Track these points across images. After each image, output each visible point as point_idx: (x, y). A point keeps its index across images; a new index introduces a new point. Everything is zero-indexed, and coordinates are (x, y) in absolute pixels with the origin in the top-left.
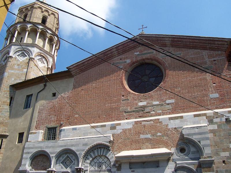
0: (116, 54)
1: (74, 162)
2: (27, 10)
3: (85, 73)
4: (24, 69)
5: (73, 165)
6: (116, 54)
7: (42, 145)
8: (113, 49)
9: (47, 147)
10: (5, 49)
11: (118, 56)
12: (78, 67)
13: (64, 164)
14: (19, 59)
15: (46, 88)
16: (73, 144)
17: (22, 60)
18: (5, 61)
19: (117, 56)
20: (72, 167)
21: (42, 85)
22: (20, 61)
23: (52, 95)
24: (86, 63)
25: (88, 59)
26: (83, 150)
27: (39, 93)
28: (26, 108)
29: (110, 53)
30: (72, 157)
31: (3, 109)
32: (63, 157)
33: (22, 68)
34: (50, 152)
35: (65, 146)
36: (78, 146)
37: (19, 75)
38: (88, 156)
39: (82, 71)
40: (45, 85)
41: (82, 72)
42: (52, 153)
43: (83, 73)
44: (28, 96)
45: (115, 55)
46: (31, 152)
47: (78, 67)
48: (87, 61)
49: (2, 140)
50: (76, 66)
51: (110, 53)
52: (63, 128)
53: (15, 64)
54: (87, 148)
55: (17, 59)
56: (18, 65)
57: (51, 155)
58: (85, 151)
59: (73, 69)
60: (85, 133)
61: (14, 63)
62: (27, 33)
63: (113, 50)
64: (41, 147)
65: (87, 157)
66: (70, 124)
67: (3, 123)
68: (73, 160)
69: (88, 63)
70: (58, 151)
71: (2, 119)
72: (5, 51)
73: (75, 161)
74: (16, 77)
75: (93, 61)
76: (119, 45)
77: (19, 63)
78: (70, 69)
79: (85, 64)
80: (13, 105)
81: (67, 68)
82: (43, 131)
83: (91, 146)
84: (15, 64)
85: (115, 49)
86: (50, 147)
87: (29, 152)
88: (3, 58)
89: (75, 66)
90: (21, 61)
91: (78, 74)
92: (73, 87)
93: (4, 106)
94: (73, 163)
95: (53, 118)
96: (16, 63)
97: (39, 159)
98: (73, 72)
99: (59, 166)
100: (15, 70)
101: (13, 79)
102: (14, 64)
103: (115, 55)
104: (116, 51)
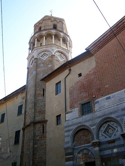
1: (117, 129)
2: (41, 24)
4: (48, 65)
5: (116, 132)
7: (80, 119)
9: (86, 122)
13: (107, 133)
14: (43, 59)
15: (72, 71)
17: (45, 59)
18: (32, 64)
20: (116, 134)
21: (67, 71)
22: (43, 60)
23: (77, 76)
29: (122, 24)
32: (104, 127)
33: (47, 65)
34: (89, 125)
35: (104, 116)
36: (117, 112)
40: (70, 70)
41: (101, 49)
42: (92, 126)
43: (101, 49)
44: (57, 84)
46: (72, 129)
47: (95, 46)
49: (43, 125)
50: (94, 45)
51: (122, 24)
52: (97, 100)
53: (41, 63)
55: (41, 59)
56: (43, 63)
59: (92, 48)
60: (120, 99)
64: (80, 123)
66: (102, 95)
67: (41, 112)
70: (98, 122)
71: (40, 108)
74: (43, 73)
75: (108, 37)
78: (89, 49)
80: (46, 95)
81: (86, 49)
82: (77, 109)
84: (41, 63)
86: (89, 121)
87: (70, 130)
89: (92, 45)
90: (44, 60)
91: (97, 52)
92: (96, 64)
93: (39, 97)
94: (116, 130)
98: (92, 51)
100: (42, 68)
101: (41, 75)
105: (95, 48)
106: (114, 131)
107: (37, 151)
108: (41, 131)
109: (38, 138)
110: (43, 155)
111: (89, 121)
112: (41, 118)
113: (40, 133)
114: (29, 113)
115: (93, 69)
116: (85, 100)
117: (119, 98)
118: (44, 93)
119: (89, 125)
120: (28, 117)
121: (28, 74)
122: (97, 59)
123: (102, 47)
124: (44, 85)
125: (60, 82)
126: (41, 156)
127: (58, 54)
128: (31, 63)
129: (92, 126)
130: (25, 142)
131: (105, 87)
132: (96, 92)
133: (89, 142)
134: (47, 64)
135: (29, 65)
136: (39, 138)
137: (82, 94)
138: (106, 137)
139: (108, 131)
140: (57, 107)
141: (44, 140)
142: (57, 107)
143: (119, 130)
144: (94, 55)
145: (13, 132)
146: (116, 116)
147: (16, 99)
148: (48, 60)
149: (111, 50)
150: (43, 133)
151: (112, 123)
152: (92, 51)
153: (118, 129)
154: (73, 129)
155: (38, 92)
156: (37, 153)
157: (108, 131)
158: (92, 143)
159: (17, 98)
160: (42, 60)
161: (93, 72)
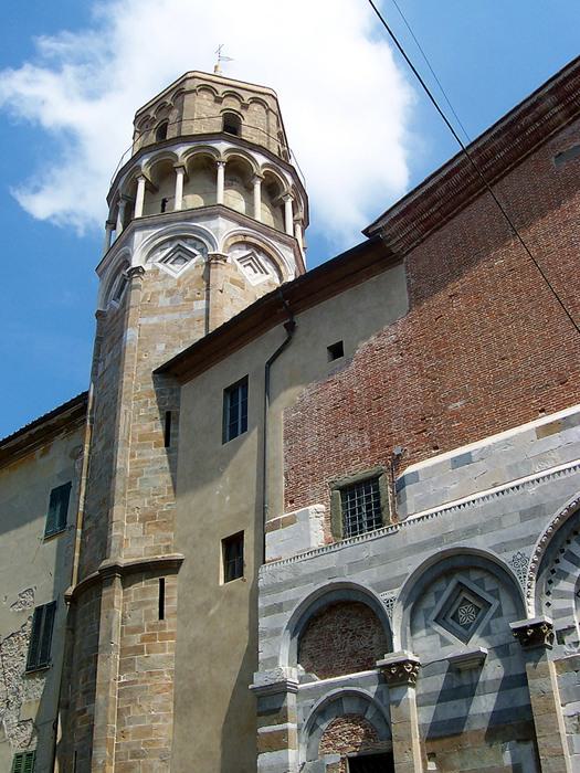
0: (560, 116)
1: (495, 604)
3: (445, 230)
6: (560, 116)
7: (331, 561)
8: (541, 100)
10: (112, 253)
11: (569, 124)
12: (409, 216)
14: (169, 272)
16: (475, 521)
18: (119, 297)
19: (565, 124)
20: (494, 629)
21: (277, 333)
23: (325, 354)
24: (442, 189)
25: (445, 173)
26: (530, 540)
27: (270, 363)
28: (234, 434)
30: (480, 583)
31: (144, 462)
32: (438, 595)
33: (187, 300)
35: (438, 541)
36: (501, 527)
37: (181, 327)
38: (557, 561)
39: (432, 226)
40: (291, 328)
45: (560, 122)
46: (292, 603)
48: (442, 181)
50: (403, 213)
52: (410, 469)
53: (159, 293)
54: (546, 525)
56: (170, 293)
57: (382, 597)
58: (538, 542)
60: (516, 465)
61: (153, 290)
62: (180, 177)
63: (543, 106)
65: (556, 566)
66: (436, 448)
67: (154, 518)
68: (489, 598)
69: (448, 190)
72: (113, 263)
73: (498, 597)
75: (468, 175)
76: (566, 74)
77: (171, 285)
78: (380, 230)
79: (436, 194)
80: (177, 443)
81: (365, 232)
83: (562, 510)
84: (159, 293)
85: (549, 101)
87: (281, 603)
88: (110, 287)
90: (177, 276)
91: (418, 244)
92: (411, 299)
94: (493, 609)
95: (355, 442)
97: (331, 627)
98: (394, 242)
99: (429, 638)
100: (163, 313)
102: (153, 293)
103: (560, 122)
104: (556, 105)
106: (484, 615)
107: (130, 702)
108: (149, 607)
109: (136, 639)
110: (156, 719)
111: (370, 563)
112: (152, 548)
113: (148, 615)
114: (96, 522)
116: (357, 471)
117: (510, 462)
118: (172, 431)
119: (371, 585)
120: (93, 540)
121: (99, 340)
122: (418, 277)
124: (171, 394)
125: (244, 383)
126: (148, 722)
128: (114, 290)
129: (385, 586)
130: (76, 656)
131: (450, 407)
132: (409, 430)
133: (368, 665)
134: (188, 296)
135: (106, 299)
136: (143, 640)
137: (342, 439)
138: (444, 642)
139: (456, 612)
140: (228, 498)
141: (164, 651)
142: (228, 498)
143: (504, 611)
144: (405, 259)
145: (23, 611)
146: (491, 545)
147: (41, 456)
148: (192, 280)
150: (161, 616)
151: (475, 575)
152: (394, 242)
153: (500, 607)
154: (298, 599)
155: (145, 427)
156: (128, 708)
157: (456, 612)
158: (382, 667)
159: (45, 452)
160: (166, 276)
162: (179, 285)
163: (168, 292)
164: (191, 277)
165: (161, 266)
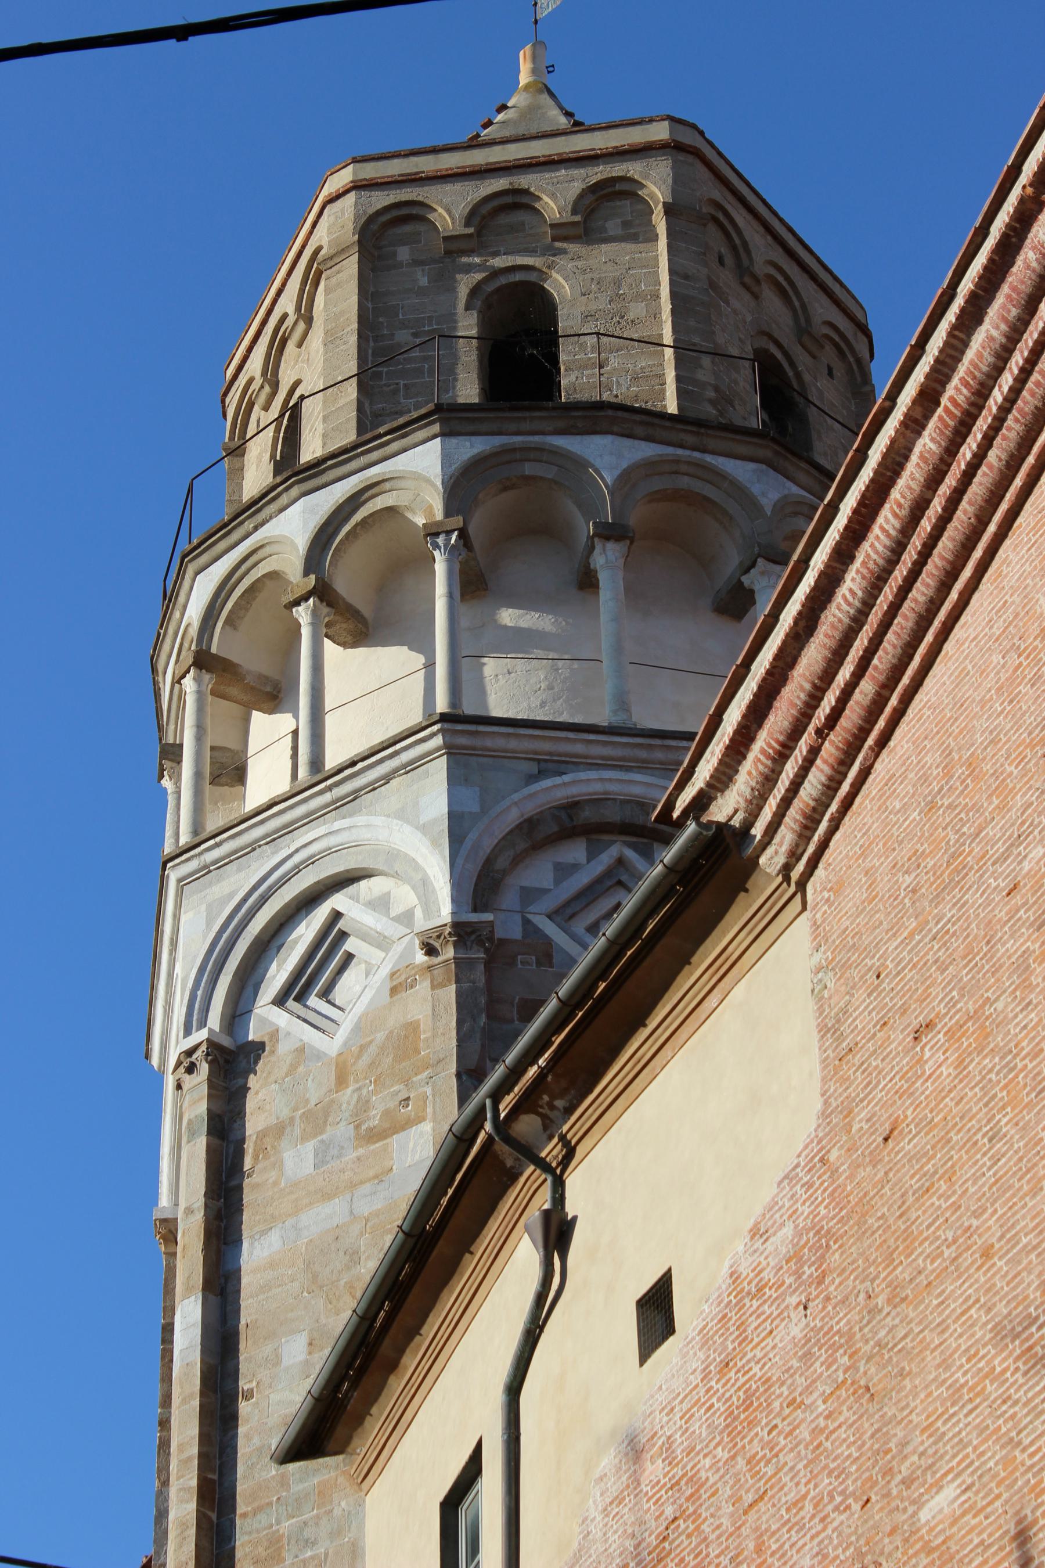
22: (319, 1055)
77: (314, 1093)
78: (702, 802)
96: (285, 1113)
105: (790, 769)
115: (789, 1177)
123: (881, 723)
127: (563, 871)
148: (382, 1048)
149: (987, 767)
161: (788, 1231)
162: (341, 1080)
163: (307, 1116)
164: (380, 1036)
165: (280, 1018)
